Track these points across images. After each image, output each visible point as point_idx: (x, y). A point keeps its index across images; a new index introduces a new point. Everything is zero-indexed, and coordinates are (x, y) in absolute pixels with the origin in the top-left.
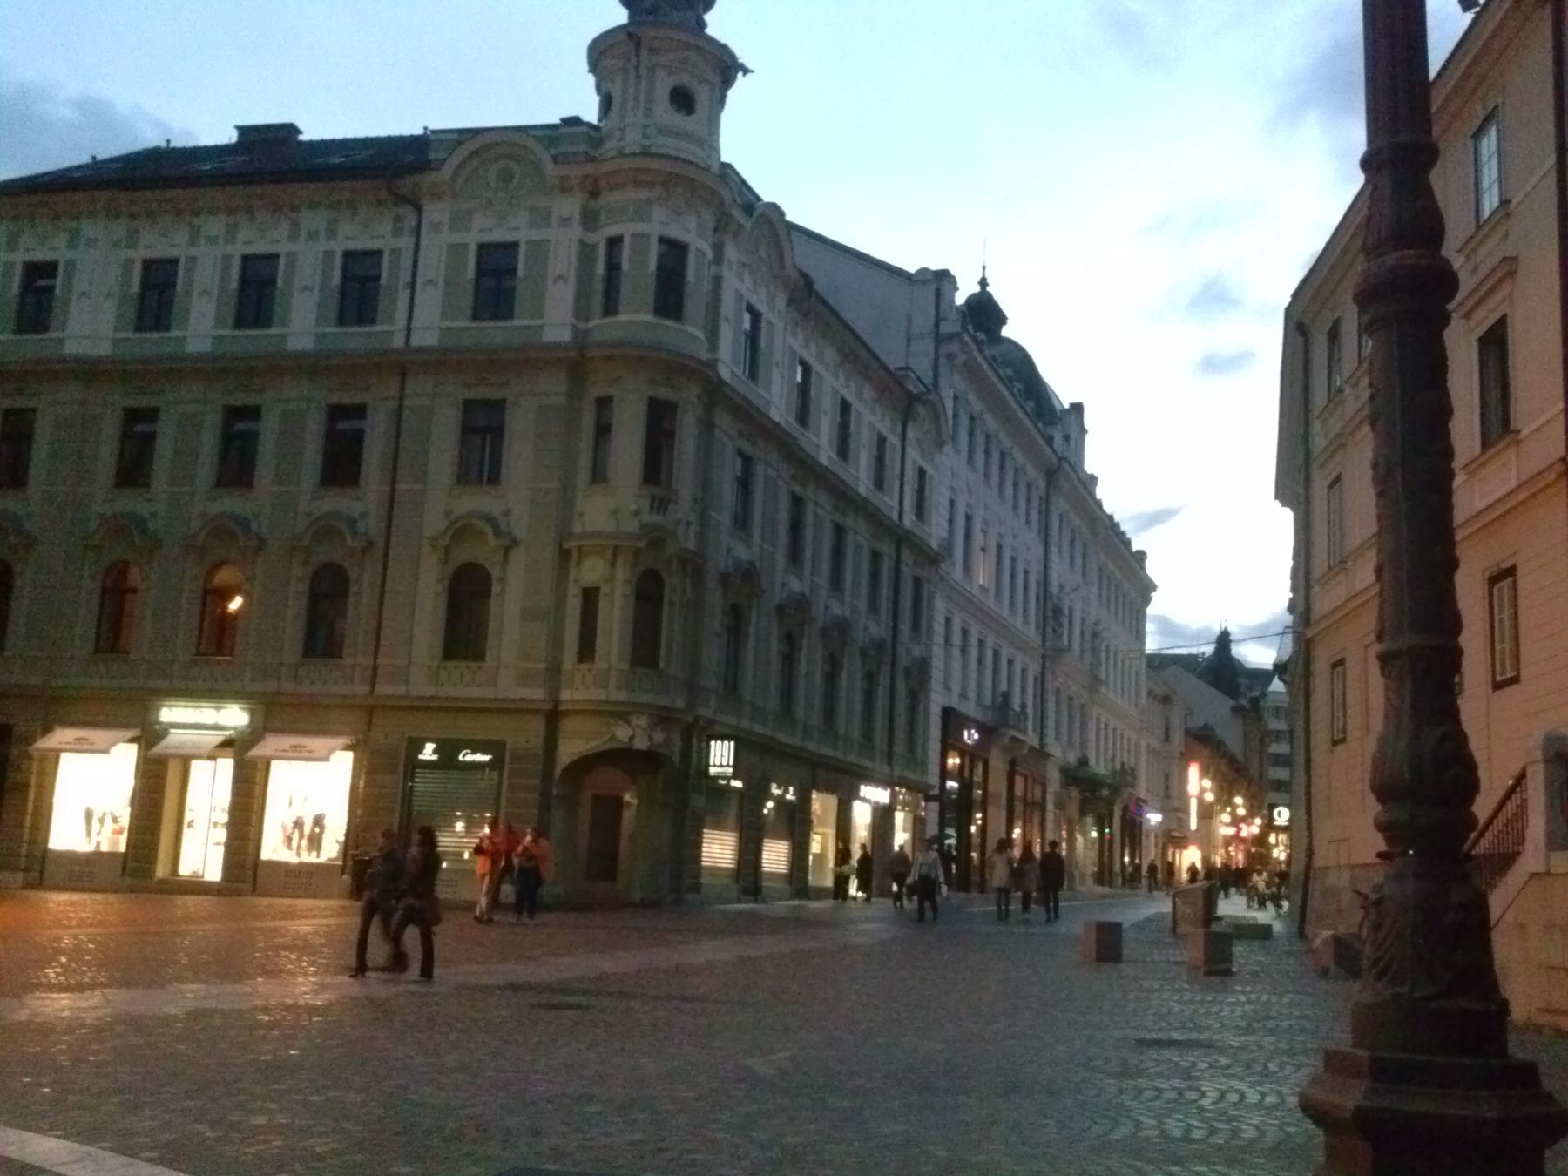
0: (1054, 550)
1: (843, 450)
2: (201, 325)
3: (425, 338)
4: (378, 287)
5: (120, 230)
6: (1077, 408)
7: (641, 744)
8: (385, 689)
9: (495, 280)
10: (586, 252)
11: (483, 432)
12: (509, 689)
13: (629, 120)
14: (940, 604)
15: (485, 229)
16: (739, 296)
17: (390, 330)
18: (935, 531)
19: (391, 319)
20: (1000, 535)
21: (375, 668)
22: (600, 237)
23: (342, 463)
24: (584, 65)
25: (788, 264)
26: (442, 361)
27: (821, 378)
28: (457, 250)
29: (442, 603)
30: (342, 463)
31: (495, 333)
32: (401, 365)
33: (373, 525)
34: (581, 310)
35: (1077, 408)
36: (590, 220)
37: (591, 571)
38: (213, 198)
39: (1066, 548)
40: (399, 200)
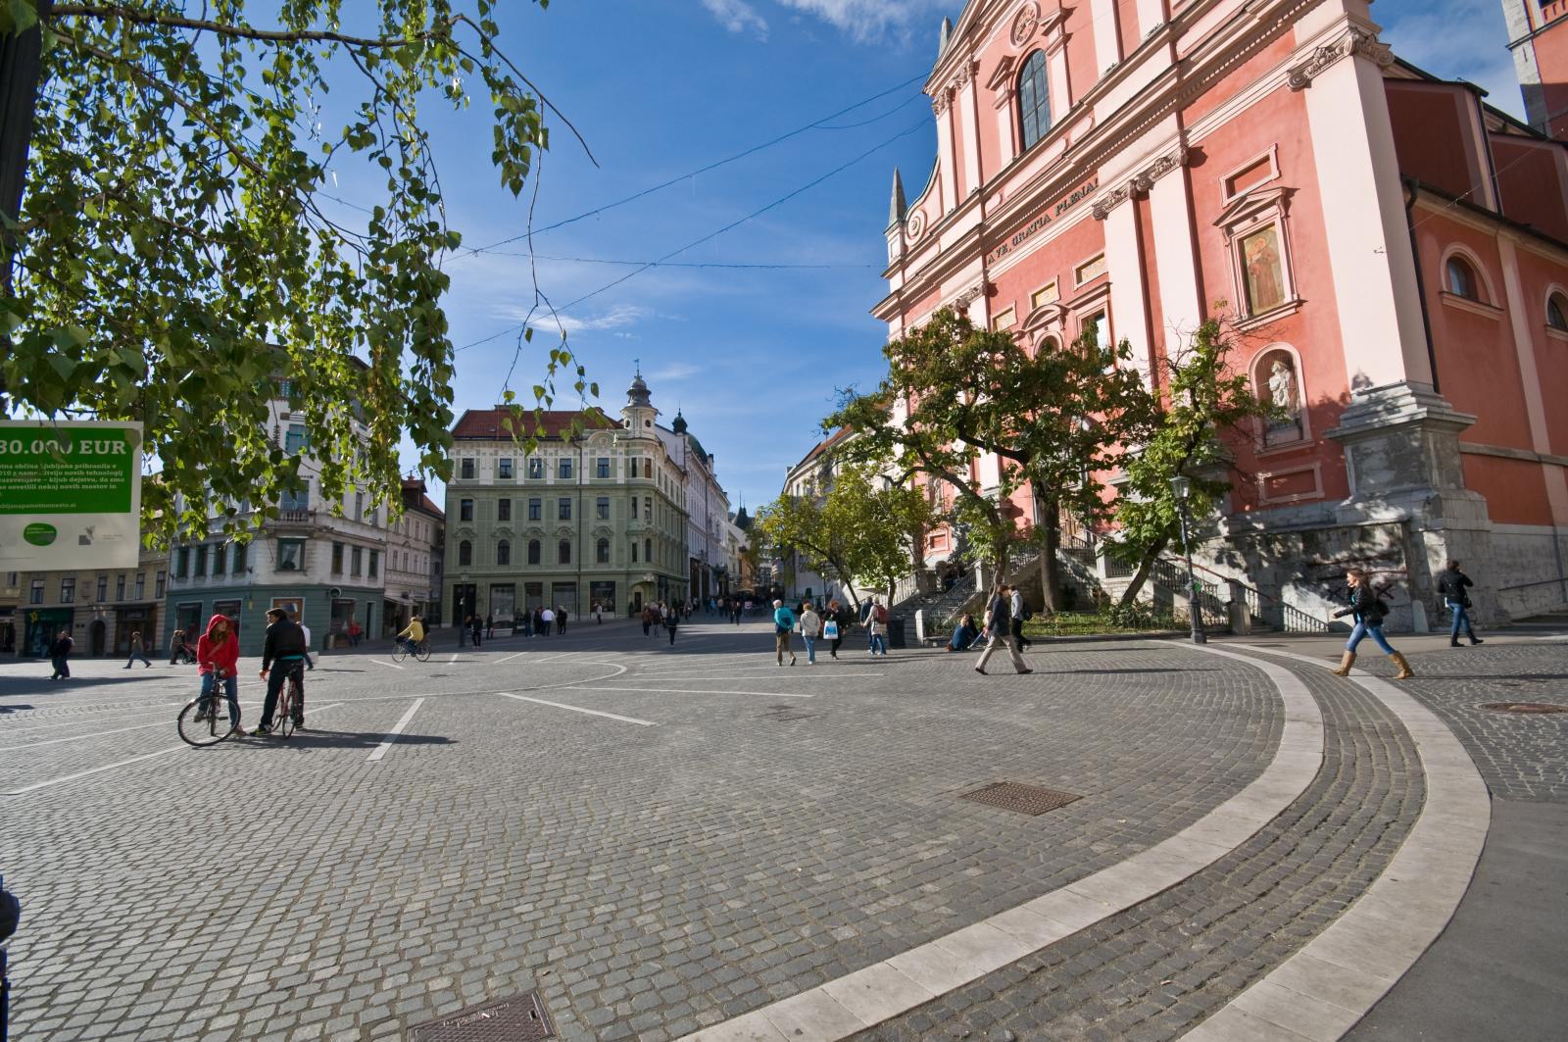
2: (550, 478)
3: (586, 482)
5: (492, 450)
6: (711, 456)
9: (603, 468)
10: (627, 460)
11: (603, 506)
12: (614, 568)
15: (599, 454)
18: (688, 509)
23: (565, 515)
24: (448, 317)
26: (592, 487)
28: (592, 460)
30: (565, 515)
31: (604, 481)
32: (580, 488)
33: (575, 530)
34: (627, 475)
35: (711, 456)
36: (627, 453)
37: (634, 540)
38: (1297, 516)
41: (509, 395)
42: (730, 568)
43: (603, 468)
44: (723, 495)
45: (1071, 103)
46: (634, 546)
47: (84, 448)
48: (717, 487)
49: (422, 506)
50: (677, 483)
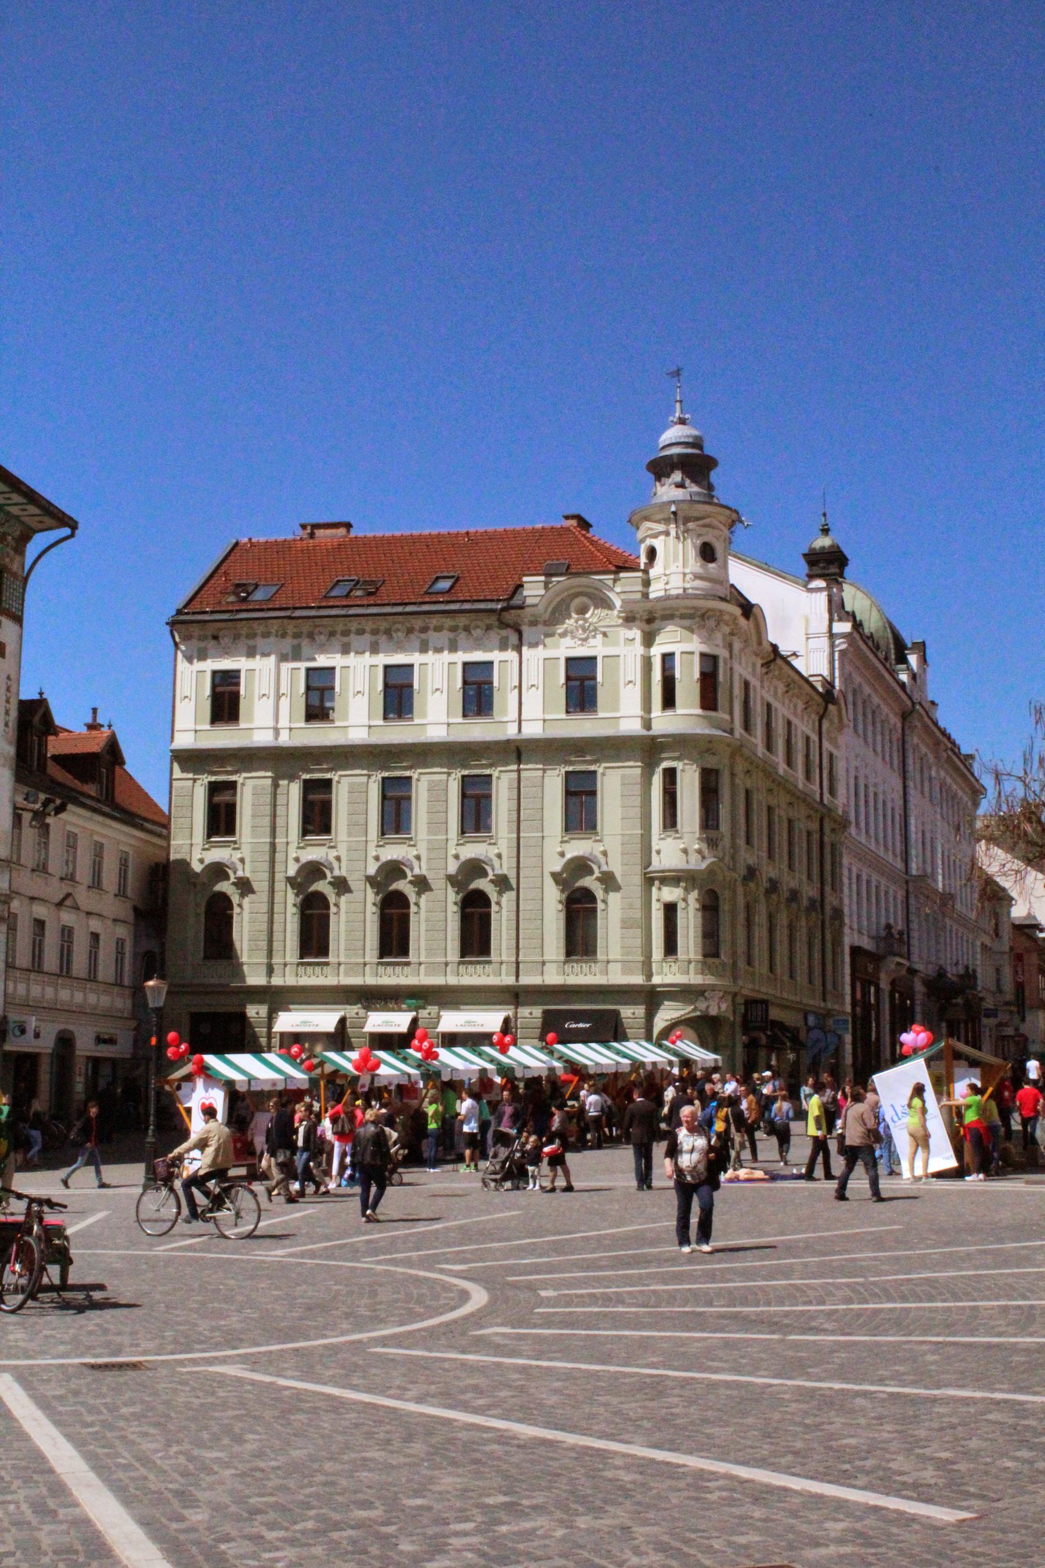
0: (911, 784)
1: (769, 746)
3: (533, 730)
4: (491, 689)
7: (713, 1011)
8: (526, 980)
9: (581, 687)
12: (617, 977)
13: (673, 568)
14: (846, 861)
16: (762, 698)
17: (503, 725)
18: (842, 800)
19: (505, 712)
20: (866, 777)
21: (518, 963)
22: (657, 651)
25: (764, 643)
27: (813, 731)
29: (562, 916)
36: (649, 640)
39: (850, 707)
40: (504, 625)
41: (41, 694)
42: (985, 978)
43: (581, 687)
44: (959, 763)
45: (185, 607)
46: (670, 910)
47: (161, 885)
48: (944, 744)
49: (121, 797)
50: (804, 727)
